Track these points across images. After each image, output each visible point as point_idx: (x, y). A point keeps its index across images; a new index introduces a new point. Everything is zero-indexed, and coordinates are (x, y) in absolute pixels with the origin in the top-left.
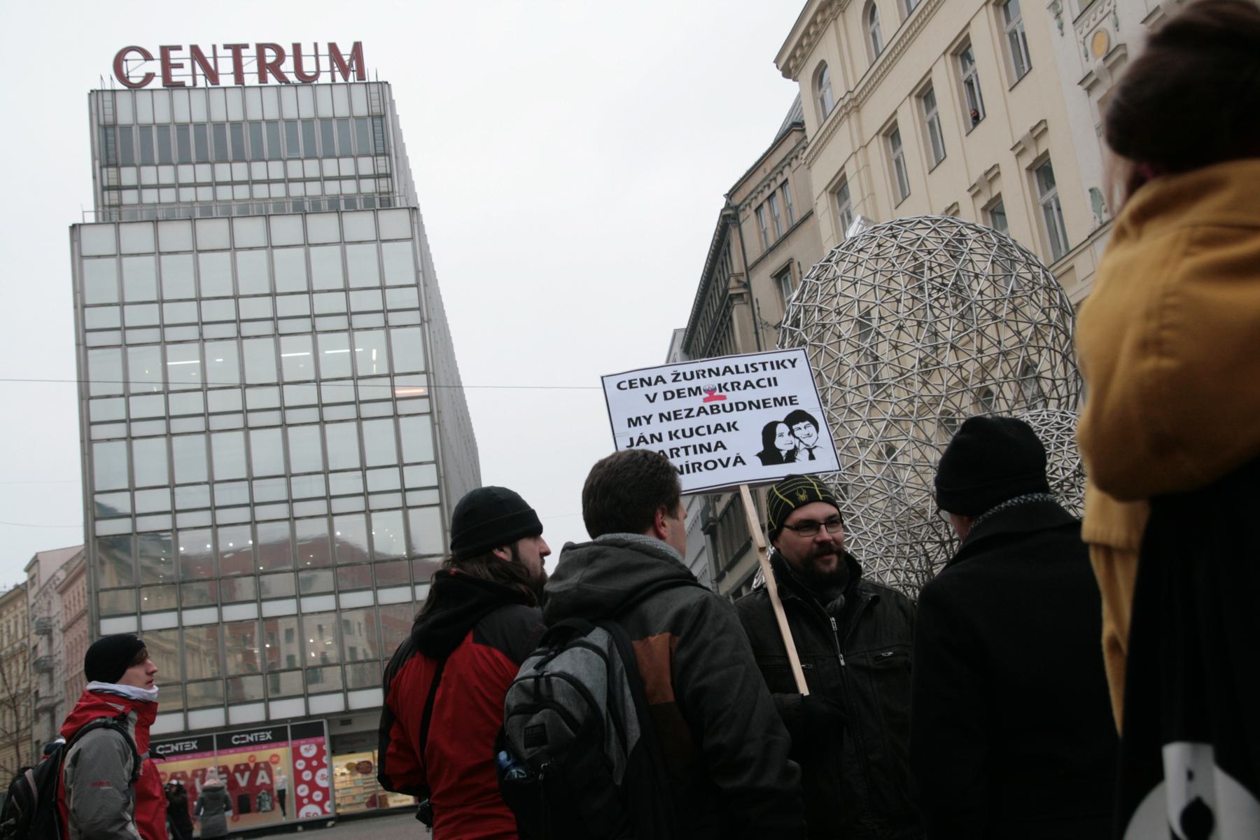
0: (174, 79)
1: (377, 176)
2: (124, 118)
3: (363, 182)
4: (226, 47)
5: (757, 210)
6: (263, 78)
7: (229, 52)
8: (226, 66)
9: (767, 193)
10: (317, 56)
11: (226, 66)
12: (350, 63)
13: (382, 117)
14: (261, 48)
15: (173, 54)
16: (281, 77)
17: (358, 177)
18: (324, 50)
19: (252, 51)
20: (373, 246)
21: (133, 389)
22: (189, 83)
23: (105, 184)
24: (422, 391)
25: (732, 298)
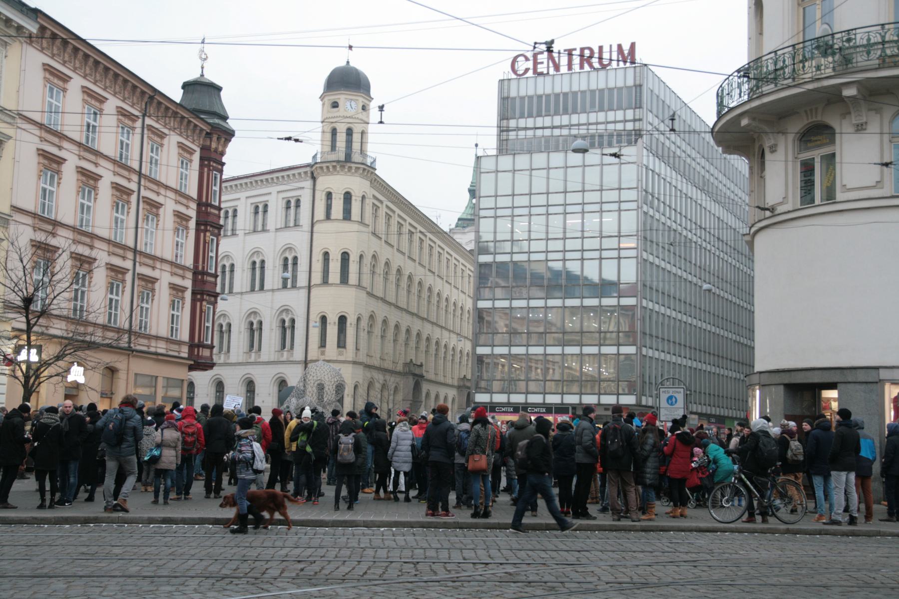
0: (539, 70)
2: (513, 94)
6: (582, 67)
12: (628, 56)
13: (641, 86)
14: (582, 50)
16: (591, 65)
17: (625, 121)
18: (615, 48)
21: (568, 235)
24: (633, 245)
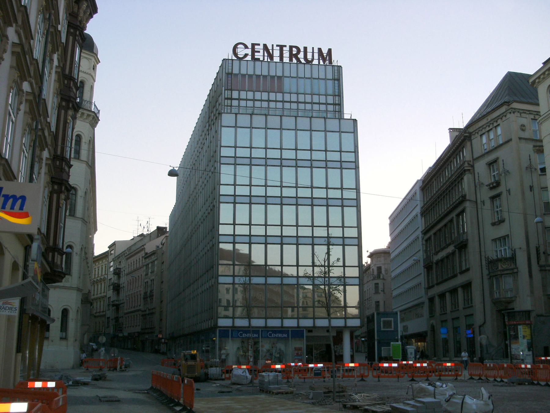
0: (256, 57)
1: (334, 104)
2: (236, 71)
3: (329, 106)
4: (277, 46)
5: (481, 136)
6: (291, 60)
7: (278, 48)
8: (277, 53)
9: (488, 129)
10: (313, 52)
11: (277, 53)
14: (291, 47)
15: (256, 47)
18: (316, 51)
19: (287, 48)
20: (338, 134)
22: (261, 59)
23: (226, 97)
25: (465, 171)
